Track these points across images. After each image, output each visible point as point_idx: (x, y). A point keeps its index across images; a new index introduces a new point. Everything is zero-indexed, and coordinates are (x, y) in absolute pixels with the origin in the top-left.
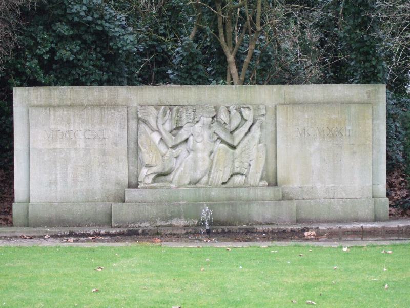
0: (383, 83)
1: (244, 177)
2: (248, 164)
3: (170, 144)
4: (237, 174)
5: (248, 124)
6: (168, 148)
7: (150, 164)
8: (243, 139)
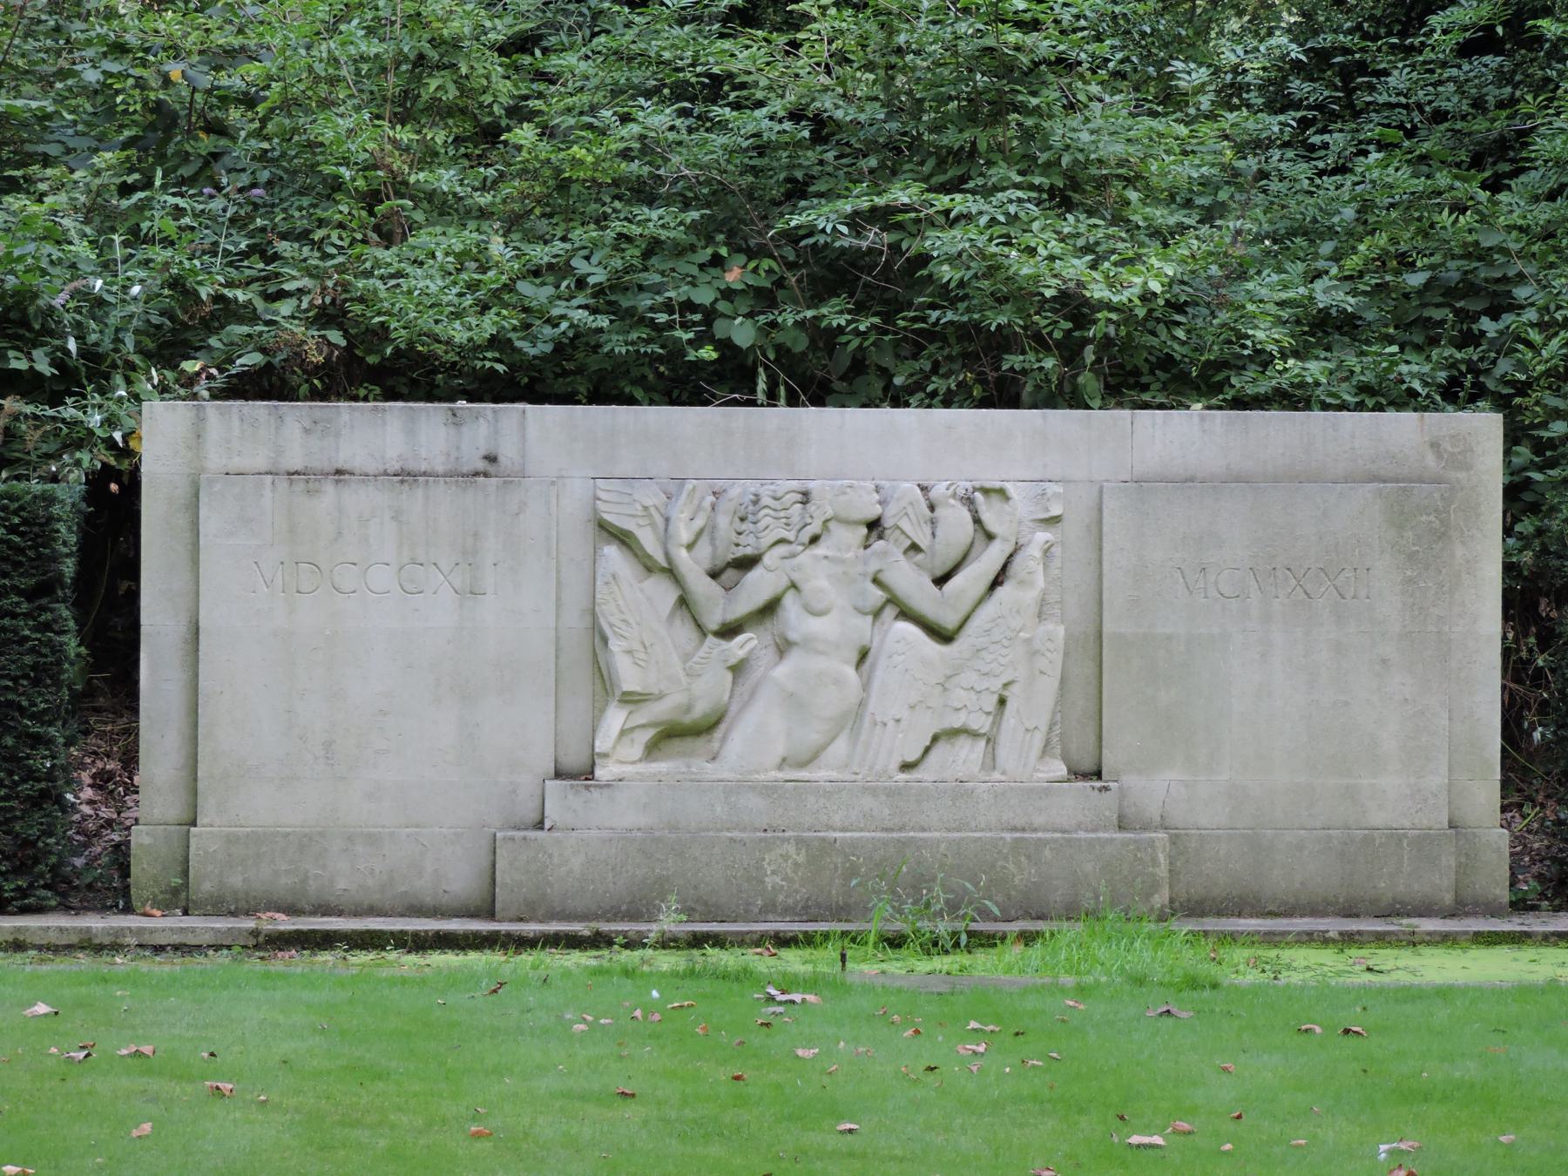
0: (115, 503)
2: (995, 698)
3: (713, 621)
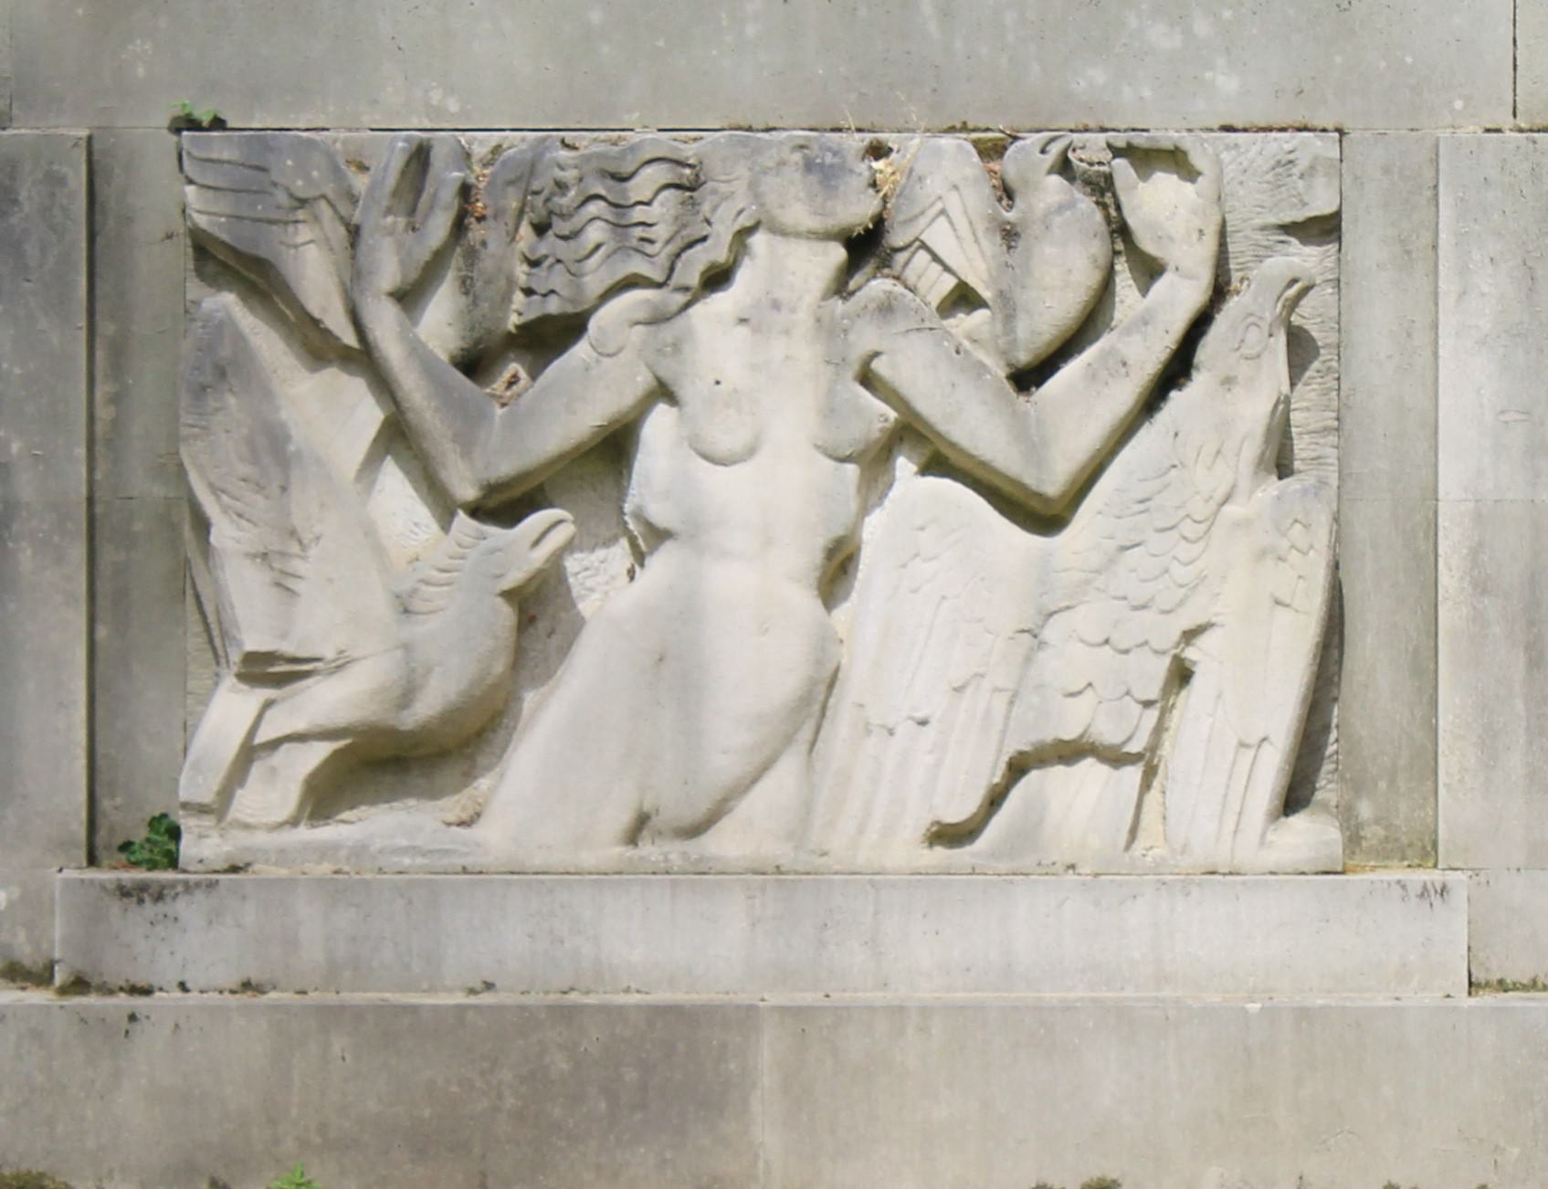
1: (1133, 774)
4: (1069, 752)
5: (1179, 296)
6: (444, 506)
7: (288, 648)
8: (1007, 718)
